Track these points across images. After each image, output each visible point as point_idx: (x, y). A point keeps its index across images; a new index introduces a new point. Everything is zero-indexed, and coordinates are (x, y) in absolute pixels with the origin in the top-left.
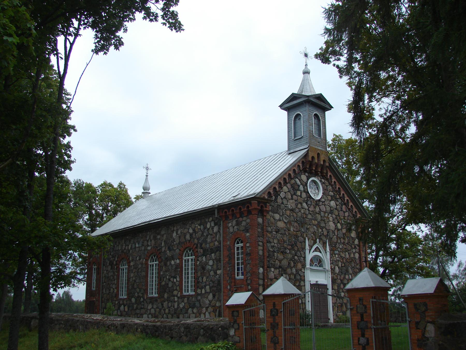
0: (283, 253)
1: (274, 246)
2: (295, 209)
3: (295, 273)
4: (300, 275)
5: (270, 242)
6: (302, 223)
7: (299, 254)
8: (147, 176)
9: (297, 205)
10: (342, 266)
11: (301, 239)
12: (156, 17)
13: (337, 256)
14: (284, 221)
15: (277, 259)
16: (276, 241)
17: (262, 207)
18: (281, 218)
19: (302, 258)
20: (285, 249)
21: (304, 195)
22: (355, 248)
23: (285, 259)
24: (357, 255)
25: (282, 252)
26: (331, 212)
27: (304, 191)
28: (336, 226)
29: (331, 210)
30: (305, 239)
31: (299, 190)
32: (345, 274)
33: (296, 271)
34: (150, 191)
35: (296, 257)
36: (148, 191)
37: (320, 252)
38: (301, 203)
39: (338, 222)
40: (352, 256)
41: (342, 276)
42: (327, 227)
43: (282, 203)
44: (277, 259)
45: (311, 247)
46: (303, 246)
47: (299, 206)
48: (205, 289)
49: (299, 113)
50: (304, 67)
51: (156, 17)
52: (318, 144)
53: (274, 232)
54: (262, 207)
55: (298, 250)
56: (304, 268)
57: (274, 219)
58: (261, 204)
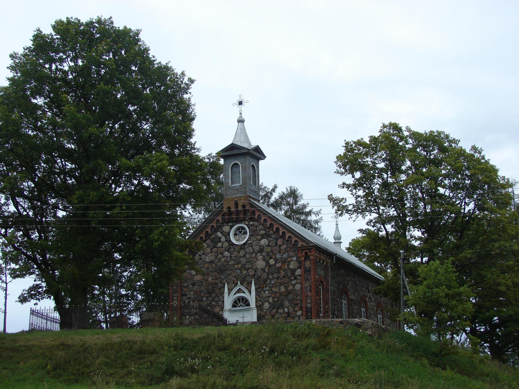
1: (190, 298)
2: (214, 260)
5: (187, 295)
6: (221, 271)
8: (337, 225)
10: (274, 301)
11: (220, 285)
13: (267, 292)
16: (192, 293)
19: (221, 302)
20: (202, 297)
26: (261, 251)
28: (268, 263)
31: (220, 241)
32: (278, 309)
34: (341, 241)
35: (213, 303)
36: (339, 241)
37: (244, 293)
39: (271, 258)
40: (290, 288)
41: (274, 311)
42: (254, 268)
43: (201, 259)
45: (230, 290)
46: (222, 292)
47: (220, 256)
49: (238, 162)
50: (239, 115)
52: (236, 192)
55: (216, 296)
56: (223, 310)
57: (191, 275)
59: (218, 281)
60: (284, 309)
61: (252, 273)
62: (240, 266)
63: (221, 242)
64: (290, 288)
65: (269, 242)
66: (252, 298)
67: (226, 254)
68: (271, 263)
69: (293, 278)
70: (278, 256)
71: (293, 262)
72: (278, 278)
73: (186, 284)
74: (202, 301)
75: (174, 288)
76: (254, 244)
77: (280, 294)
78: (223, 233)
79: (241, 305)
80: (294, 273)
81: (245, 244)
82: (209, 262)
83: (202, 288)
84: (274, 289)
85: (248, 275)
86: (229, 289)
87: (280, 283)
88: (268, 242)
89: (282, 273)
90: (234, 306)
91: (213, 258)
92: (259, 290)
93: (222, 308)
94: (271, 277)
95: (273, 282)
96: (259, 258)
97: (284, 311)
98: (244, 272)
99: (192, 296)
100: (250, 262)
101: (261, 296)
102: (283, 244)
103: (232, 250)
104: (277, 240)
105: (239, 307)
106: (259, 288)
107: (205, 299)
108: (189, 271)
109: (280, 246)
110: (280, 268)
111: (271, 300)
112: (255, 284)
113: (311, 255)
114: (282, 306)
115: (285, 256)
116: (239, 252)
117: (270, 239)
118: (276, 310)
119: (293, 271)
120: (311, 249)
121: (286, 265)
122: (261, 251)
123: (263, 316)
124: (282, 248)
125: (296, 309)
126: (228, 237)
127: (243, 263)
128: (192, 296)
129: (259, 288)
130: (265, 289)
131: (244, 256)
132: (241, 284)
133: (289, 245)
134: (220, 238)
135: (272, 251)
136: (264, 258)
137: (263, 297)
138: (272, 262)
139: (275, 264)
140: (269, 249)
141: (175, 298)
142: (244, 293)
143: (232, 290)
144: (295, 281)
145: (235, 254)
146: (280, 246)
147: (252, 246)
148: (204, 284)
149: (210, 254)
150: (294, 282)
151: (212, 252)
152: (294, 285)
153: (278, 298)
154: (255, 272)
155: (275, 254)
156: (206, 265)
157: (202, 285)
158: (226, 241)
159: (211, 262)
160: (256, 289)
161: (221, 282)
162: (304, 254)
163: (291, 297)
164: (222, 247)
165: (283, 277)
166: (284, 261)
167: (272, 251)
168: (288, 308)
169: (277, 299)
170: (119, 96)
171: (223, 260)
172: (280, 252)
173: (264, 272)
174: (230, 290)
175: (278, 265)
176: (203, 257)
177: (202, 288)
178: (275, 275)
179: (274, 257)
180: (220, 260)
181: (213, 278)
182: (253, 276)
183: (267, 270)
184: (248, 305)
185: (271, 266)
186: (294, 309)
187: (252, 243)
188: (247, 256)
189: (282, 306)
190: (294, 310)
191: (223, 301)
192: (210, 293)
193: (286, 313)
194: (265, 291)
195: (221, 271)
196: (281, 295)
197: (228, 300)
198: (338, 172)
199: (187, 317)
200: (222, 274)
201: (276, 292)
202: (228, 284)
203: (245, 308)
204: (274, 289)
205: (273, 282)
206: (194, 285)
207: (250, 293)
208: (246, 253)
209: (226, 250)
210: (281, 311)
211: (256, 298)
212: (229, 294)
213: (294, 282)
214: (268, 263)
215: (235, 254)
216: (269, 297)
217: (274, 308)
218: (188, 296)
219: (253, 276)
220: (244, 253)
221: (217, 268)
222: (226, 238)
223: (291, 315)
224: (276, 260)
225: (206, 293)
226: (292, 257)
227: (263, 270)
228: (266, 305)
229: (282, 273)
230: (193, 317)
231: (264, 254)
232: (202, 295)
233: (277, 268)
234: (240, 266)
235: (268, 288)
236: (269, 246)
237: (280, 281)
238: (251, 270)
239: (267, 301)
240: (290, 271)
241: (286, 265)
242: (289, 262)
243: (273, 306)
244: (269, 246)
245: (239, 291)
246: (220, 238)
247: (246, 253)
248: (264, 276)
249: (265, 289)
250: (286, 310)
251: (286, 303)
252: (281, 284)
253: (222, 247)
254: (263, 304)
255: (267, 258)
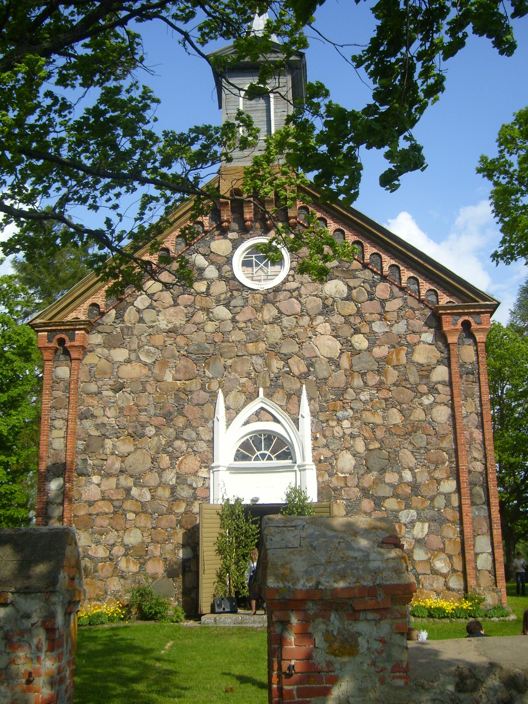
0: (136, 436)
2: (183, 327)
3: (173, 482)
4: (190, 486)
5: (93, 416)
6: (203, 356)
7: (189, 434)
9: (189, 318)
12: (464, 33)
13: (346, 424)
14: (141, 361)
15: (113, 454)
17: (61, 342)
18: (133, 357)
19: (202, 446)
20: (143, 426)
21: (220, 288)
22: (433, 390)
23: (139, 451)
24: (442, 414)
25: (129, 435)
26: (327, 310)
27: (221, 277)
29: (325, 306)
30: (214, 395)
32: (383, 471)
33: (178, 476)
37: (276, 420)
38: (207, 310)
39: (357, 331)
43: (141, 320)
44: (113, 454)
46: (206, 415)
47: (200, 316)
48: (352, 388)
51: (464, 33)
53: (104, 393)
54: (61, 342)
55: (188, 425)
56: (209, 468)
58: (58, 336)
59: (195, 385)
60: (399, 473)
61: (298, 366)
62: (262, 346)
63: (202, 279)
64: (419, 414)
65: (350, 289)
66: (302, 437)
67: (222, 312)
68: (357, 346)
69: (424, 388)
70: (378, 327)
71: (422, 345)
72: (379, 387)
73: (93, 387)
74: (142, 436)
75: (59, 393)
76: (303, 291)
77: (388, 430)
78: (212, 256)
79: (263, 456)
80: (428, 377)
81: (277, 290)
82: (169, 331)
83: (144, 400)
84: (368, 416)
85: (288, 373)
86: (227, 408)
87: (386, 400)
88: (345, 289)
89: (393, 375)
90: (240, 456)
91: (179, 321)
92: (322, 417)
93: (207, 462)
94: (358, 382)
95: (365, 396)
96: (319, 330)
97: (401, 477)
98: (276, 364)
99: (113, 421)
100: (293, 337)
101: (327, 433)
102: (393, 297)
103: (237, 302)
104: (374, 285)
105: (257, 459)
106: (322, 410)
107: (150, 431)
108: (106, 351)
109: (383, 302)
110: (386, 360)
111: (360, 446)
112: (310, 399)
113: (477, 330)
114: (393, 462)
115: (400, 327)
116: (258, 310)
117: (352, 283)
118: (375, 473)
119: (425, 371)
120: (479, 313)
121: (403, 354)
122: (327, 310)
123: (335, 489)
124: (389, 306)
125: (438, 474)
126: (226, 268)
127: (272, 340)
128: (113, 421)
129: (322, 410)
130: (340, 414)
131: (276, 321)
132: (269, 395)
133: (410, 300)
134: (201, 270)
135: (359, 313)
136: (335, 329)
137: (333, 436)
138: (360, 342)
139: (369, 350)
140: (351, 308)
141: (58, 423)
142: (276, 420)
143: (238, 411)
144: (432, 399)
145: (247, 313)
146: (383, 302)
147: (300, 295)
148: (149, 388)
149: (172, 310)
150: (427, 401)
151: (176, 304)
152: (428, 409)
153: (381, 441)
154: (311, 365)
155: (369, 323)
156: (159, 340)
157: (144, 390)
158: (221, 277)
159: (173, 331)
160: (314, 414)
161: (203, 388)
162: (459, 326)
163: (420, 439)
164: (207, 293)
165: (394, 385)
166: (396, 344)
167: (359, 313)
168: (411, 469)
169: (377, 445)
170: (4, 30)
171: (210, 327)
172: (383, 316)
173: (338, 366)
174: (232, 412)
175: (380, 351)
176: (148, 316)
177: (144, 400)
178: (373, 379)
179: (366, 329)
180: (200, 327)
181: (180, 376)
182: (303, 377)
183: (345, 363)
184: (288, 455)
185: (355, 352)
186: (429, 473)
187: (298, 289)
188: (286, 321)
189: (393, 462)
190: (432, 478)
191: (211, 442)
192: (168, 417)
193: (408, 484)
194: (339, 421)
195: (203, 356)
196: (392, 434)
197: (228, 436)
198: (218, 420)
199: (96, 479)
200: (208, 365)
201: (376, 425)
202: (226, 395)
203: (275, 463)
204: (368, 416)
205: (365, 396)
206: (118, 388)
207: (296, 422)
208: (280, 312)
209: (218, 302)
210: (391, 478)
211: (315, 439)
212: (228, 426)
213: (427, 401)
214: (347, 343)
215: (247, 313)
216: (352, 436)
217: (369, 470)
218: (99, 421)
219: (303, 377)
220: (275, 312)
221: (192, 348)
222: (219, 269)
223: (424, 491)
224: (373, 340)
225: (155, 415)
226: (420, 333)
227: (334, 362)
228: (347, 461)
229: (393, 375)
230: (113, 481)
231: (337, 319)
232: (143, 417)
233: (378, 360)
234: (262, 346)
235: (351, 412)
236: (349, 298)
237: (384, 394)
238: (296, 358)
239: (347, 449)
240: (414, 369)
241: (403, 354)
242: (412, 347)
243: (365, 464)
244: (349, 298)
245: (258, 415)
246: (201, 270)
247: (280, 312)
248: (339, 379)
249: (340, 414)
250: (408, 476)
251: (407, 457)
252: (390, 403)
253: (207, 293)
254: (335, 456)
255: (346, 331)
